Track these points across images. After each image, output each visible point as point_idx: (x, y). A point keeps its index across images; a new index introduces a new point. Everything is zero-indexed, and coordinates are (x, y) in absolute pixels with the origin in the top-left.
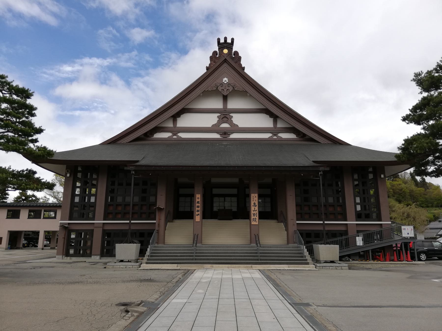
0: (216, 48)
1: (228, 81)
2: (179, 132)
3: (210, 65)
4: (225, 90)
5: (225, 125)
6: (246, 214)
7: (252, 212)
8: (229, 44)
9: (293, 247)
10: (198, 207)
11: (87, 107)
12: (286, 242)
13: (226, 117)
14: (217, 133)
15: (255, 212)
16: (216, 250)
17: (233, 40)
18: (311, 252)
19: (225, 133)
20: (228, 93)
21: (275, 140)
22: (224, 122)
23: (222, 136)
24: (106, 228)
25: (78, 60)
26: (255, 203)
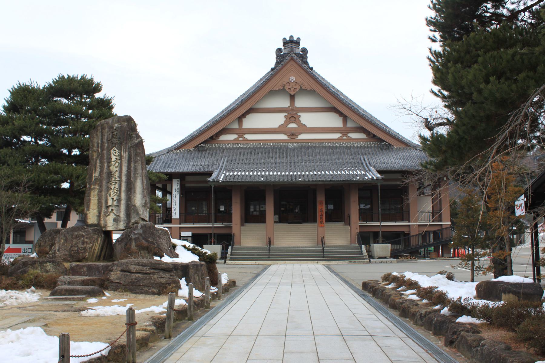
1: (294, 80)
2: (245, 134)
4: (292, 89)
5: (293, 126)
9: (354, 247)
12: (350, 242)
13: (293, 117)
14: (285, 133)
16: (287, 250)
19: (293, 134)
20: (296, 92)
22: (291, 122)
23: (290, 137)
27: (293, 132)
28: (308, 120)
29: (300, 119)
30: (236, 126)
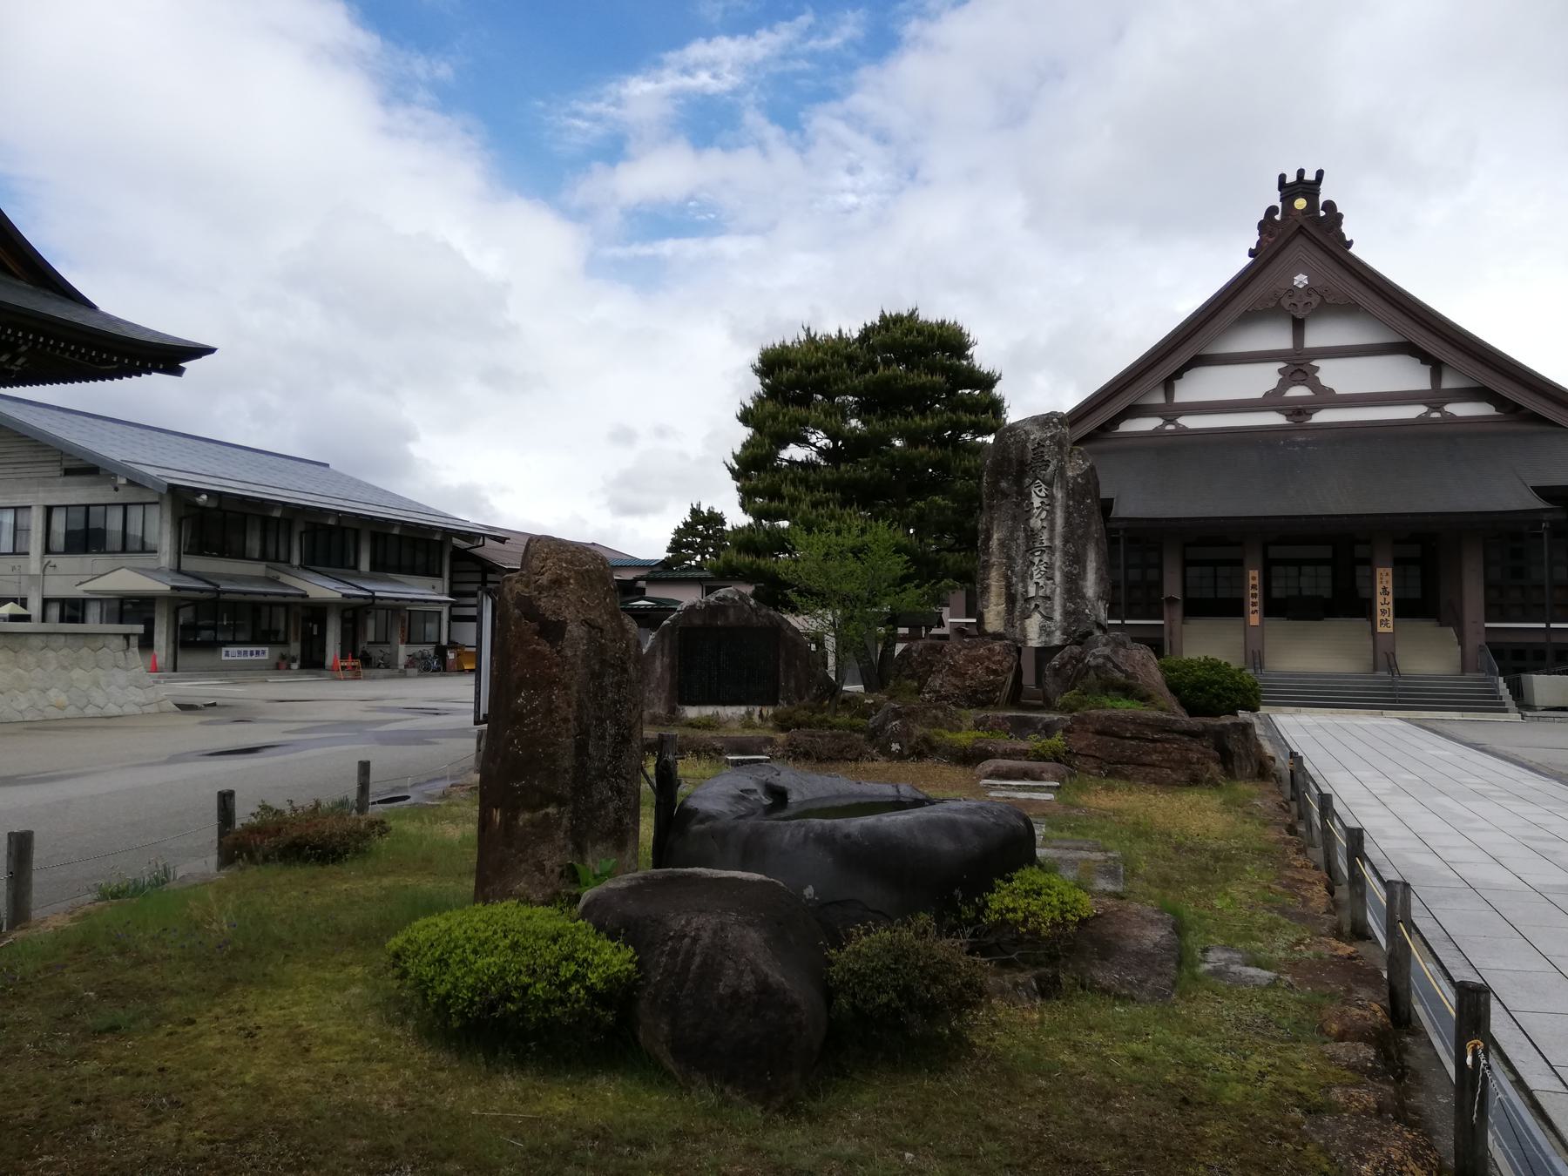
0: (1275, 199)
3: (1258, 243)
4: (1300, 305)
6: (1365, 609)
7: (1379, 607)
8: (1309, 183)
10: (1254, 596)
11: (712, 216)
12: (1460, 670)
14: (1279, 411)
15: (1385, 607)
17: (1320, 174)
18: (1518, 693)
19: (1298, 411)
21: (1435, 422)
24: (59, 540)
25: (672, 56)
26: (1385, 588)
27: (1300, 406)
28: (1336, 376)
29: (1317, 375)
30: (1159, 399)
